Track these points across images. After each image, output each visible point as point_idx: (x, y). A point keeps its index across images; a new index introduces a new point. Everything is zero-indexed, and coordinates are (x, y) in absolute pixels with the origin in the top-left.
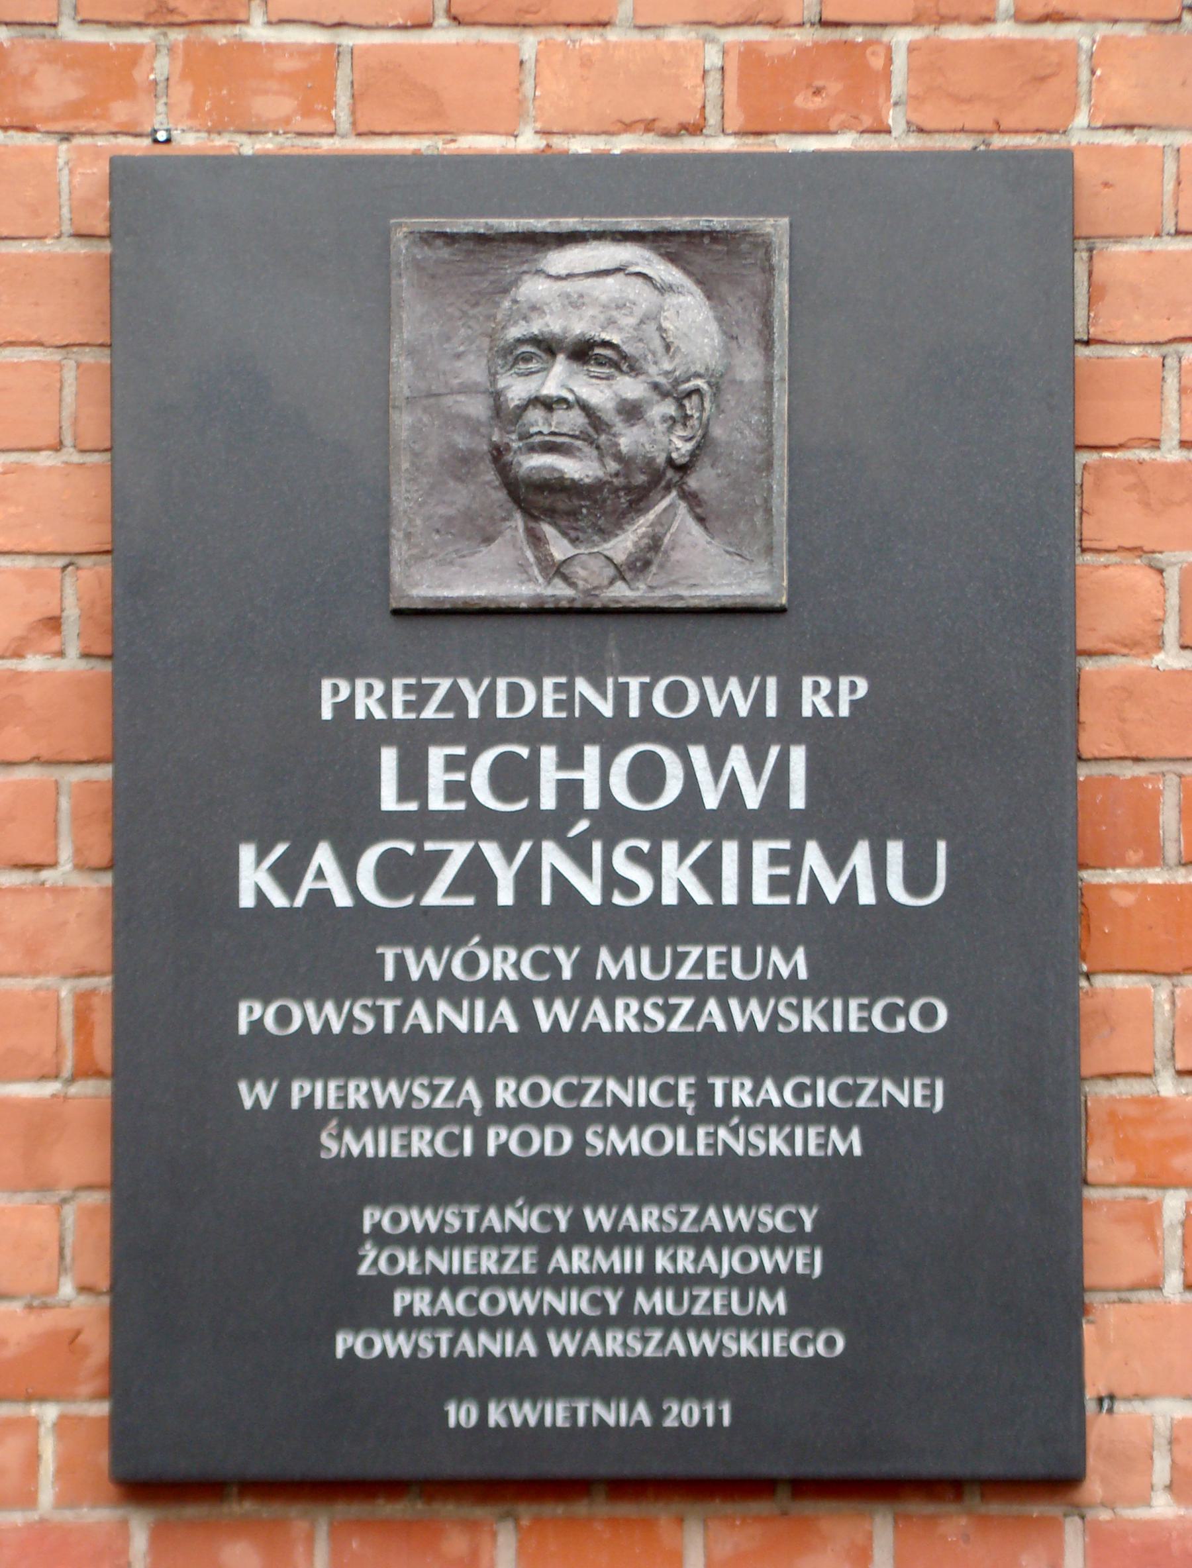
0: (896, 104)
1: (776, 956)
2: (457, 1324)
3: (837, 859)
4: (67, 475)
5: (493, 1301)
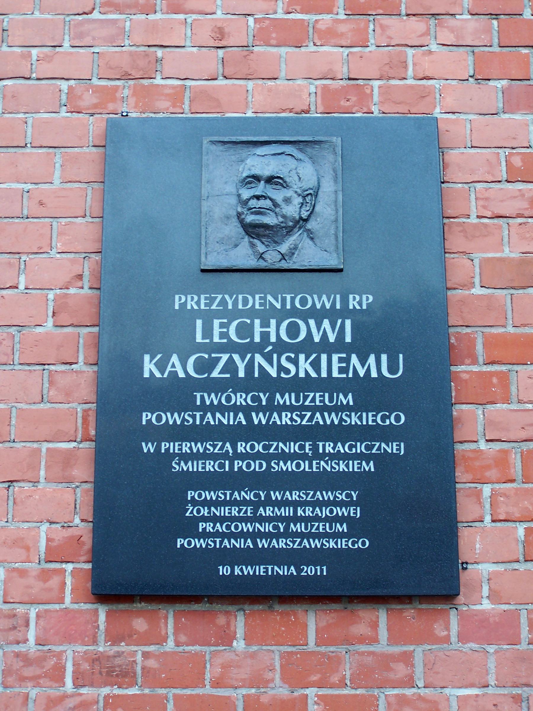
0: (375, 104)
1: (341, 396)
2: (223, 536)
3: (363, 361)
4: (87, 226)
5: (236, 527)
